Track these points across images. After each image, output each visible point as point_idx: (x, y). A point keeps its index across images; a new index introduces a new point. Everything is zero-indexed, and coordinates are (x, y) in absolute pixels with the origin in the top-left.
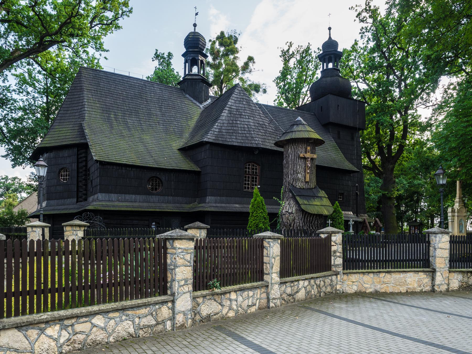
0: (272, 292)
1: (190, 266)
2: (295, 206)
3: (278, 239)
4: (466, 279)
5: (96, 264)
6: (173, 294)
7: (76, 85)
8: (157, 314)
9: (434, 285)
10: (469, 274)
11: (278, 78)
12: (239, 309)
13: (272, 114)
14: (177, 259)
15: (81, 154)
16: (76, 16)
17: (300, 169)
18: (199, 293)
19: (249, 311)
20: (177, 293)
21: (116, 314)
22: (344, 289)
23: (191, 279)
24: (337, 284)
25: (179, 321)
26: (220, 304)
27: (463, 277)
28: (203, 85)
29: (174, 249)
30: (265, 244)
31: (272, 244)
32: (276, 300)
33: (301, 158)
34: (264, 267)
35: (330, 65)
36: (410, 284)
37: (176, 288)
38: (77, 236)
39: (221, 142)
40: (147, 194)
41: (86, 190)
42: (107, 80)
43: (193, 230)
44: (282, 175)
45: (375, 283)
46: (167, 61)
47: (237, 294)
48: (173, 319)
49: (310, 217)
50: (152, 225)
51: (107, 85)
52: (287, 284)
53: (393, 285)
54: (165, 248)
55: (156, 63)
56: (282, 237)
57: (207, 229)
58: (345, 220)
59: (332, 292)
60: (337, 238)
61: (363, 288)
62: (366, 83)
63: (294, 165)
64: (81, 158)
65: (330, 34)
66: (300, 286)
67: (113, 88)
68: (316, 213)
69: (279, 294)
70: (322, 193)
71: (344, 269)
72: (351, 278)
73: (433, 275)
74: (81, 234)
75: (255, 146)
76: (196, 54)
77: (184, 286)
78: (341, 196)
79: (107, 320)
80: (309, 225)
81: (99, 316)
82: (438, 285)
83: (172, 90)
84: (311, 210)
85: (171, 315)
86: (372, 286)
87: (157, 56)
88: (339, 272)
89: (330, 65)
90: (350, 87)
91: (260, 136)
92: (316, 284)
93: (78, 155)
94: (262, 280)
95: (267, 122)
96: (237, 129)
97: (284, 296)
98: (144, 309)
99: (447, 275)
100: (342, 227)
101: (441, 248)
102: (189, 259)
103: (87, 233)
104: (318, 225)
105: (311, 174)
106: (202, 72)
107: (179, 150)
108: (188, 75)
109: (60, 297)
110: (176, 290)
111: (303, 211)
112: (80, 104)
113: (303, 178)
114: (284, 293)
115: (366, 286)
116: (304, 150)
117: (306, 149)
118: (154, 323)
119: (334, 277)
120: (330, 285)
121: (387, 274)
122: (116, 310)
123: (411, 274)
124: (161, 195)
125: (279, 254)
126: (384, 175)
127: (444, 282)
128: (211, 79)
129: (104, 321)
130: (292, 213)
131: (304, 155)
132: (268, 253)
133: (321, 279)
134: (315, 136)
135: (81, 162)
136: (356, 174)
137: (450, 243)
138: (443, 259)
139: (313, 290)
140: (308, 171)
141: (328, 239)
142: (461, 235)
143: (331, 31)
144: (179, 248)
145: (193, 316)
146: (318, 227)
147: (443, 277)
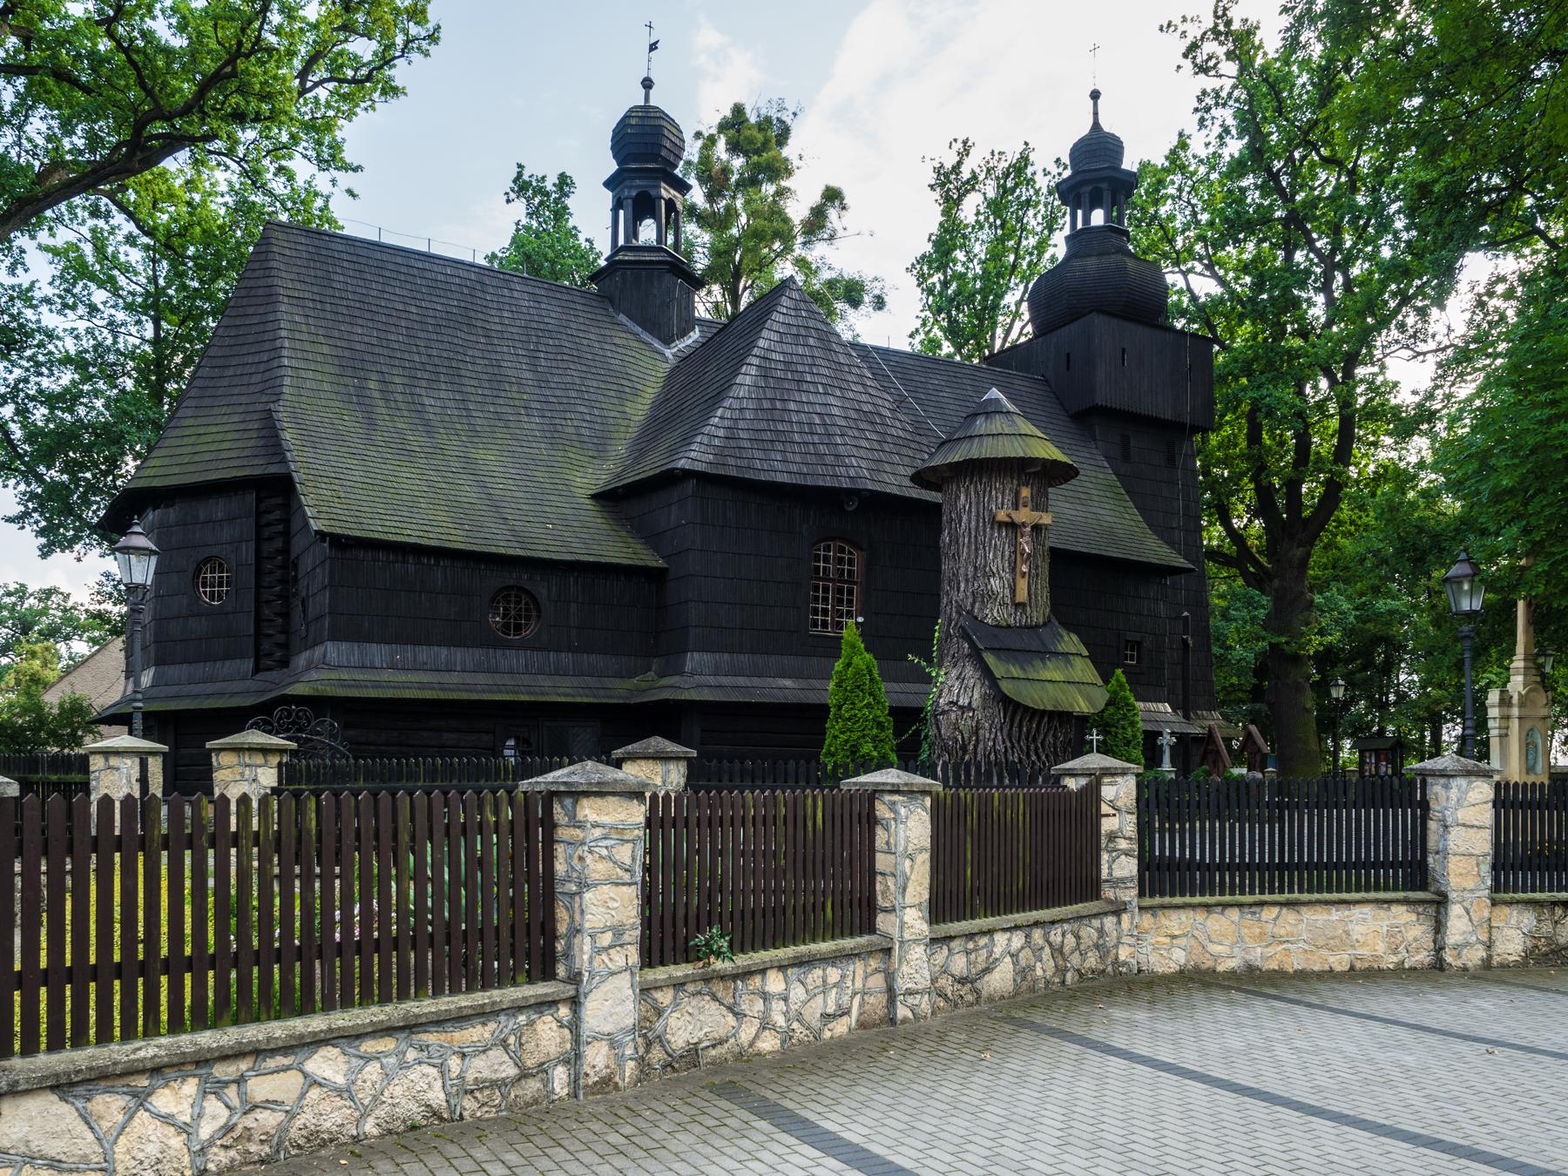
0: (905, 969)
1: (630, 884)
2: (979, 685)
3: (924, 793)
4: (1547, 928)
5: (319, 876)
6: (575, 978)
7: (252, 283)
8: (521, 1045)
9: (1442, 948)
10: (1559, 911)
11: (923, 259)
12: (795, 1025)
13: (905, 380)
14: (589, 859)
15: (269, 512)
16: (252, 52)
17: (996, 561)
18: (660, 974)
19: (827, 1034)
20: (587, 974)
21: (387, 1044)
22: (1142, 959)
23: (633, 928)
24: (1119, 943)
25: (594, 1067)
26: (730, 1009)
27: (1539, 921)
28: (675, 284)
29: (579, 827)
30: (882, 810)
31: (903, 811)
32: (918, 996)
33: (1001, 524)
34: (878, 887)
35: (1098, 218)
36: (1364, 945)
37: (586, 957)
38: (254, 785)
39: (733, 473)
40: (488, 646)
41: (285, 631)
42: (357, 267)
43: (643, 763)
44: (938, 583)
45: (1247, 939)
46: (556, 201)
47: (786, 976)
48: (573, 1059)
49: (1031, 720)
50: (504, 747)
51: (355, 282)
52: (953, 944)
53: (1306, 947)
54: (550, 825)
55: (519, 209)
56: (937, 786)
57: (689, 760)
58: (1144, 732)
59: (1104, 971)
60: (1120, 792)
61: (1207, 956)
62: (1215, 276)
63: (977, 549)
64: (268, 525)
65: (1096, 114)
66: (998, 951)
67: (375, 293)
68: (1050, 708)
69: (928, 978)
70: (1070, 642)
71: (1141, 894)
72: (1167, 923)
73: (1438, 912)
74: (268, 777)
75: (846, 484)
76: (650, 178)
77: (611, 951)
78: (1132, 650)
79: (355, 1062)
80: (1028, 747)
81: (330, 1048)
82: (1456, 947)
83: (570, 298)
84: (1034, 697)
85: (568, 1046)
86: (1236, 950)
87: (522, 186)
88: (1125, 903)
89: (1098, 218)
90: (1164, 290)
91: (863, 453)
92: (1050, 944)
93: (258, 514)
94: (871, 929)
95: (887, 404)
96: (786, 427)
97: (942, 982)
98: (479, 1026)
99: (1486, 914)
100: (1137, 753)
101: (1464, 825)
102: (628, 861)
103: (288, 774)
104: (1055, 748)
105: (1032, 577)
106: (670, 239)
107: (594, 497)
108: (623, 248)
109: (200, 985)
110: (586, 965)
111: (1006, 702)
112: (267, 346)
113: (1007, 592)
114: (945, 972)
115: (1216, 949)
116: (1008, 498)
117: (1017, 494)
118: (512, 1071)
119: (1109, 922)
120: (1097, 946)
121: (1285, 910)
122: (386, 1030)
123: (1367, 910)
124: (534, 649)
125: (927, 843)
126: (1276, 583)
127: (1474, 938)
128: (701, 262)
129: (344, 1067)
130: (970, 707)
131: (1009, 516)
132: (892, 841)
133: (1066, 926)
134: (1047, 450)
135: (270, 539)
136: (1183, 579)
137: (1494, 806)
138: (1473, 861)
139: (1038, 964)
140: (1025, 569)
141: (1091, 794)
142: (1530, 779)
143: (1100, 102)
144: (595, 825)
145: (641, 1050)
146: (1055, 754)
147: (1470, 920)
